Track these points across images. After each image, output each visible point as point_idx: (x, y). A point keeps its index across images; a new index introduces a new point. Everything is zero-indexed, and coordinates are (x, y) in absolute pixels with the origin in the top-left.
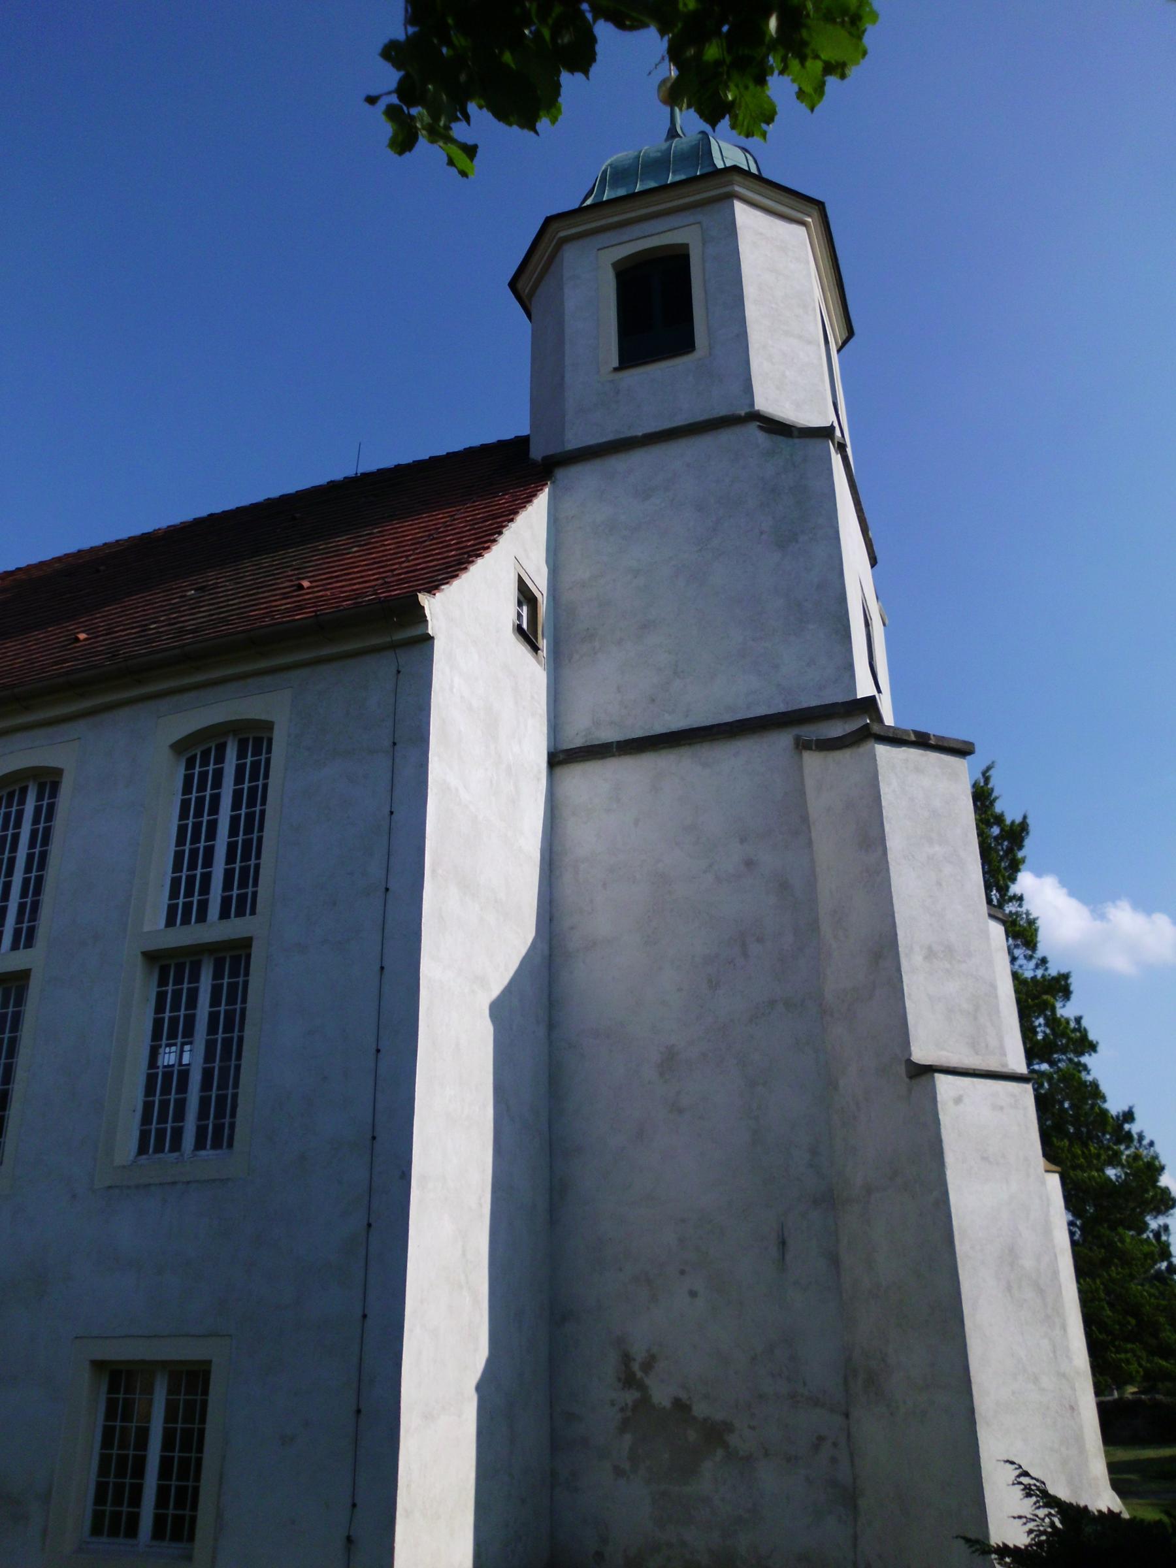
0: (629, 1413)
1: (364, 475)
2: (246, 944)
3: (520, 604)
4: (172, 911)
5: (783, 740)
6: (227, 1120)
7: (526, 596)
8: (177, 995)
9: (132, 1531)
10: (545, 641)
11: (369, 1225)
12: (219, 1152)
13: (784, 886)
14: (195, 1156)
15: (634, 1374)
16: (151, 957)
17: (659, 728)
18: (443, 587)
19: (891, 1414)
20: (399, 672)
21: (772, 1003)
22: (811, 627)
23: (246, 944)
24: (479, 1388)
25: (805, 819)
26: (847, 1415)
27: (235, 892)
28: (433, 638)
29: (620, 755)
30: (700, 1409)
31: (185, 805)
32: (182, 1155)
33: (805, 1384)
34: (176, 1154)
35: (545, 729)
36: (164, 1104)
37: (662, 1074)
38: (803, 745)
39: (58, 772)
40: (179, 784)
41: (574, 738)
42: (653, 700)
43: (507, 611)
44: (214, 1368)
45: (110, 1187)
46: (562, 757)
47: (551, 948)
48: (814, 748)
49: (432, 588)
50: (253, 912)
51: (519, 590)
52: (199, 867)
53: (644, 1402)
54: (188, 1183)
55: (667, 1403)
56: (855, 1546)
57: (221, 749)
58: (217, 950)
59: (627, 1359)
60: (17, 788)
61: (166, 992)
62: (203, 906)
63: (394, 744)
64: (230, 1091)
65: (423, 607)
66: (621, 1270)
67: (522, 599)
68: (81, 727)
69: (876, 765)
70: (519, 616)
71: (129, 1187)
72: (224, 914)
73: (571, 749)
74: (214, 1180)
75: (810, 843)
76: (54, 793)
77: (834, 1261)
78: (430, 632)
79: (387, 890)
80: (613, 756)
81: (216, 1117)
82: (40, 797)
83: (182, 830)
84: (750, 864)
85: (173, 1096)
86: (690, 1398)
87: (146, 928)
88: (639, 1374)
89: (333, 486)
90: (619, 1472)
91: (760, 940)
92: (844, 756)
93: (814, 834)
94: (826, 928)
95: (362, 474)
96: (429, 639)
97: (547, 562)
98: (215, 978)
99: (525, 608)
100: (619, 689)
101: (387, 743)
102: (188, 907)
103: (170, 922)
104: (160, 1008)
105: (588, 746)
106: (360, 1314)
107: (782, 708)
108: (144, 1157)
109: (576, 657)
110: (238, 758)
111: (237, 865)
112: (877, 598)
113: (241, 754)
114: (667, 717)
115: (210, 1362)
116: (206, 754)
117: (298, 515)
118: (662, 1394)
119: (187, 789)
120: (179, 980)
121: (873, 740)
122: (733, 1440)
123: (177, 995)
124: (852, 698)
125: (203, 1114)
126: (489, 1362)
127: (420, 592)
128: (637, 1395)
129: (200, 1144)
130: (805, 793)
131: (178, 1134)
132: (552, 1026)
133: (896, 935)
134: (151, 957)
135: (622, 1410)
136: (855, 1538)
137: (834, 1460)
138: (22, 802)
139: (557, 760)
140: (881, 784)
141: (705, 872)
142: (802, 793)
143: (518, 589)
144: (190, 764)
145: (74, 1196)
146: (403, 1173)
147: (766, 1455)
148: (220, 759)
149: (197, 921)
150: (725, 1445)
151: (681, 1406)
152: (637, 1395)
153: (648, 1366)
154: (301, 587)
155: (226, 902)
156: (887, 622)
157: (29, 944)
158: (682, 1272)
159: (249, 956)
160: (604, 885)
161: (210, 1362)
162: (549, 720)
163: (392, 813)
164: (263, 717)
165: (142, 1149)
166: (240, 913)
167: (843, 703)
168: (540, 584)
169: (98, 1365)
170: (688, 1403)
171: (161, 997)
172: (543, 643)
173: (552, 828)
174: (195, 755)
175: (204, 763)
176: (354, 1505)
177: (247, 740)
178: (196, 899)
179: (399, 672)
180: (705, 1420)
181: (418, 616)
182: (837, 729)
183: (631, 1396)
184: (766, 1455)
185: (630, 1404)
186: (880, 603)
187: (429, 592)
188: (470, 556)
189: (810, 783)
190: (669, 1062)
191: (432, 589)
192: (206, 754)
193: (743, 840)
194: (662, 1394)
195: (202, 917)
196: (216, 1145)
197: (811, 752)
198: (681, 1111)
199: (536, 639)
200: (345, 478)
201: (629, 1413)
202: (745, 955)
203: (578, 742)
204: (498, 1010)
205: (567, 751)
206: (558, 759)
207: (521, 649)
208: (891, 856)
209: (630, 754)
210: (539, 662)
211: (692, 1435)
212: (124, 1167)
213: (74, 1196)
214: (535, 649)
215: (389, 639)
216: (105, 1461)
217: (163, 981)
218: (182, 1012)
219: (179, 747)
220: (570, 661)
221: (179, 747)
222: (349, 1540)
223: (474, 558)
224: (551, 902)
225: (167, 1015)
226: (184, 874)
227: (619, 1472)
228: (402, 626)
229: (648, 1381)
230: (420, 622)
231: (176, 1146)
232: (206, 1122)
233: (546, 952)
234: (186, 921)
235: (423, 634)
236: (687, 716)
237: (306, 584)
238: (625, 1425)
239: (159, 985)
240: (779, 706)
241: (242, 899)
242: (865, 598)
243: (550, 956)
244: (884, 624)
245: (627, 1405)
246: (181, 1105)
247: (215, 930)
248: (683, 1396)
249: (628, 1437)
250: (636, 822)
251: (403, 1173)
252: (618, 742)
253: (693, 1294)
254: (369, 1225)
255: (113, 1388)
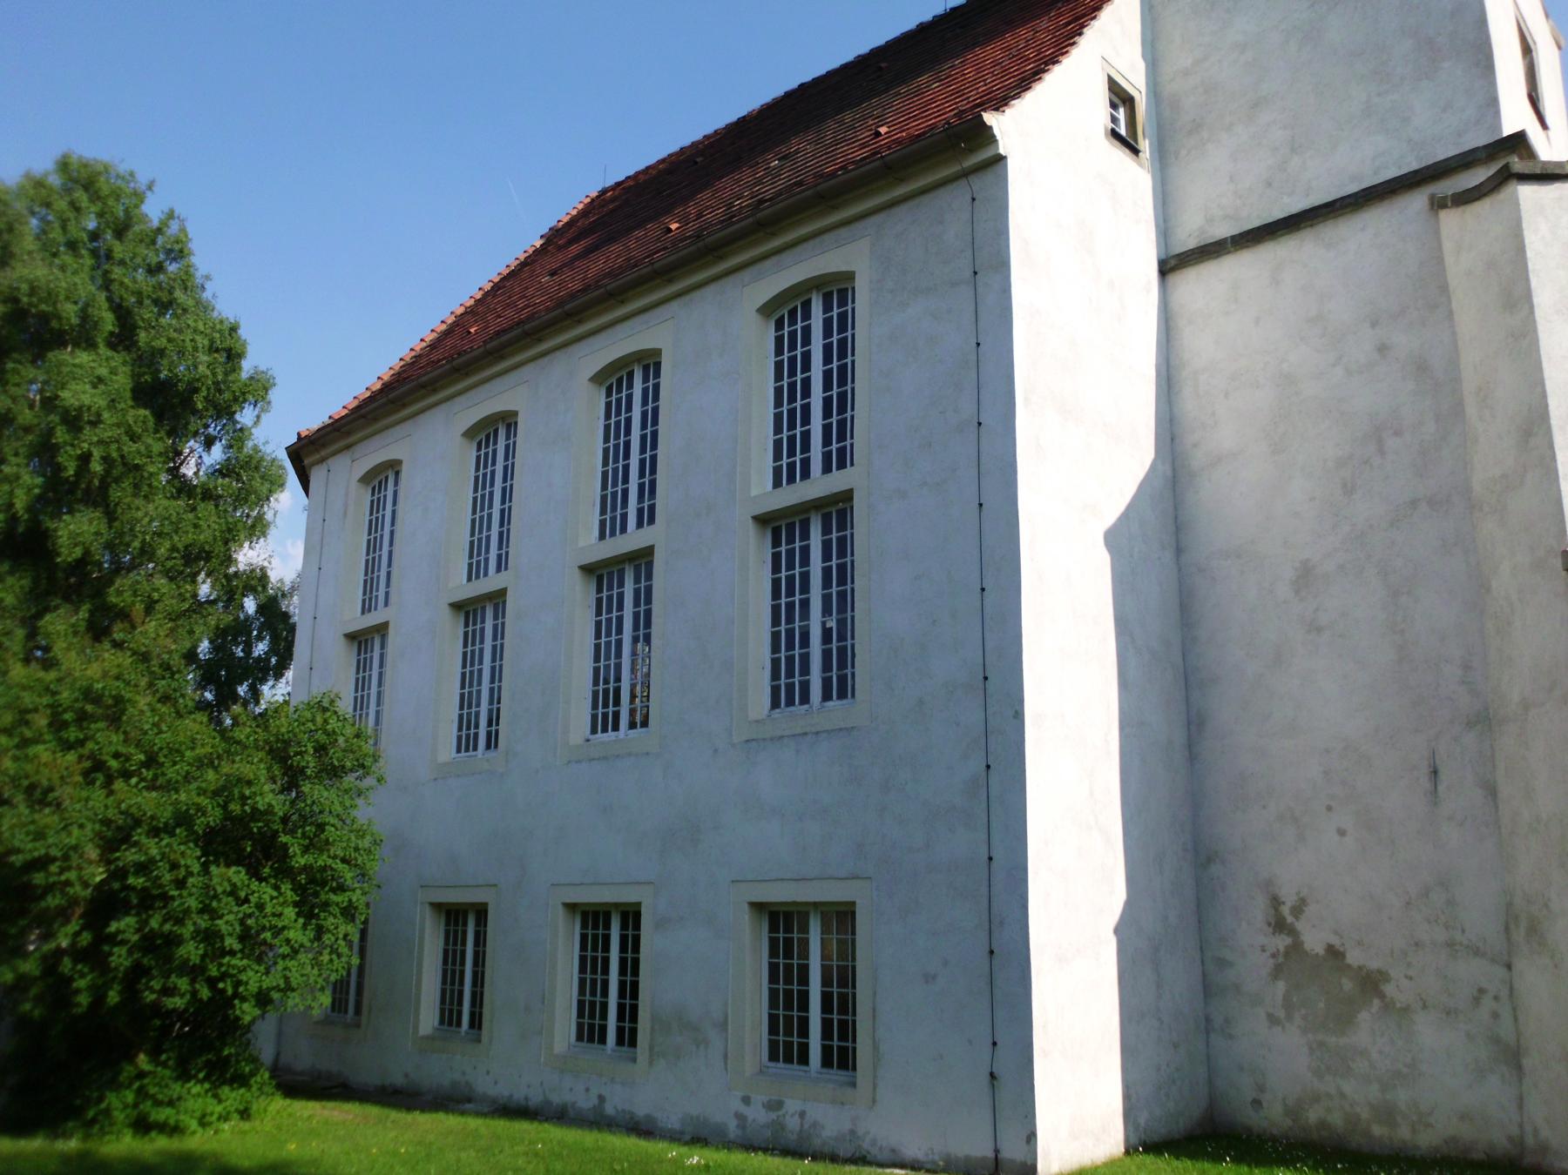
0: (1281, 960)
1: (954, 10)
2: (847, 496)
3: (1114, 106)
4: (777, 472)
5: (1417, 201)
6: (849, 671)
7: (1120, 97)
8: (791, 553)
9: (804, 1059)
10: (1147, 142)
11: (988, 767)
12: (844, 701)
13: (1421, 367)
14: (823, 707)
15: (1284, 919)
16: (762, 520)
17: (1279, 214)
18: (1013, 102)
19: (1556, 966)
20: (974, 199)
21: (1414, 503)
22: (1446, 65)
23: (847, 496)
24: (1116, 931)
25: (1444, 289)
26: (1509, 967)
27: (834, 446)
28: (1005, 157)
29: (1236, 250)
30: (1354, 957)
31: (779, 366)
32: (811, 707)
33: (1463, 931)
34: (806, 706)
35: (1153, 236)
36: (790, 660)
37: (1297, 592)
38: (1438, 204)
39: (657, 353)
40: (771, 346)
41: (1186, 240)
42: (1269, 185)
43: (1099, 112)
44: (643, 910)
45: (747, 741)
46: (1173, 262)
47: (1174, 470)
48: (1449, 204)
49: (1000, 102)
50: (852, 464)
51: (1110, 89)
52: (798, 426)
53: (1296, 947)
54: (817, 733)
55: (1320, 949)
56: (1521, 1106)
57: (807, 305)
58: (818, 505)
59: (1276, 902)
60: (624, 373)
61: (780, 553)
62: (806, 464)
63: (975, 273)
64: (849, 642)
65: (991, 128)
66: (1264, 807)
67: (1116, 100)
68: (675, 306)
69: (1519, 211)
70: (1114, 120)
71: (764, 739)
72: (827, 469)
73: (1182, 254)
74: (841, 729)
75: (1450, 314)
76: (657, 374)
77: (1492, 791)
78: (1002, 151)
79: (980, 424)
80: (1229, 252)
81: (838, 669)
82: (646, 379)
83: (778, 392)
84: (1382, 349)
85: (797, 652)
86: (1343, 944)
87: (754, 492)
88: (1290, 919)
89: (923, 29)
90: (1273, 1020)
91: (1397, 433)
92: (1483, 207)
93: (1454, 305)
94: (1471, 410)
95: (951, 9)
96: (1000, 159)
97: (1144, 56)
98: (824, 534)
99: (1122, 110)
100: (1232, 179)
101: (968, 273)
102: (791, 466)
103: (777, 483)
104: (776, 568)
105: (1202, 247)
106: (986, 857)
107: (1415, 166)
108: (777, 710)
109: (1183, 152)
110: (825, 312)
111: (834, 420)
112: (1547, 16)
113: (827, 308)
114: (1286, 200)
115: (639, 904)
116: (793, 313)
117: (883, 65)
118: (1314, 940)
119: (779, 350)
120: (791, 540)
121: (1515, 181)
122: (1389, 989)
123: (791, 553)
124: (1499, 138)
125: (826, 666)
126: (1129, 905)
127: (985, 110)
128: (1288, 941)
129: (827, 696)
130: (1443, 259)
131: (805, 687)
132: (1179, 551)
133: (1547, 406)
134: (762, 520)
135: (1273, 956)
136: (1521, 1098)
137: (1495, 1015)
138: (630, 386)
139: (1169, 266)
140: (1526, 233)
141: (1334, 365)
142: (1440, 260)
143: (1109, 89)
144: (779, 325)
145: (716, 751)
146: (1016, 712)
147: (1425, 1007)
148: (807, 315)
149: (801, 480)
150: (1382, 996)
151: (1334, 953)
152: (1288, 941)
153: (1298, 910)
154: (878, 134)
155: (827, 457)
156: (1563, 43)
157: (652, 520)
158: (1329, 808)
159: (852, 508)
160: (1226, 395)
161: (639, 904)
162: (1157, 226)
163: (978, 344)
164: (844, 269)
165: (775, 704)
166: (842, 465)
167: (1485, 147)
168: (1136, 81)
169: (758, 907)
170: (1342, 949)
171: (776, 558)
172: (1144, 145)
173: (1168, 341)
174: (783, 316)
175: (793, 322)
176: (994, 1044)
177: (831, 293)
178: (798, 458)
179: (974, 199)
180: (1360, 968)
181: (986, 136)
182: (1477, 176)
183: (1282, 942)
184: (1425, 1007)
185: (1282, 949)
186: (1550, 21)
187: (997, 109)
188: (1046, 65)
189: (1448, 246)
190: (1305, 576)
191: (1000, 103)
192: (793, 313)
193: (1374, 325)
194: (1314, 940)
195: (806, 474)
196: (842, 695)
197: (1448, 210)
198: (1319, 630)
199: (1136, 141)
200: (934, 17)
201: (1281, 960)
202: (1382, 452)
203: (1191, 244)
204: (1113, 538)
205: (1178, 255)
206: (1168, 267)
207: (1120, 155)
208: (1539, 314)
209: (1247, 247)
210: (1141, 165)
211: (1347, 984)
212: (757, 721)
213: (716, 751)
214: (1135, 151)
215: (959, 168)
216: (773, 995)
217: (776, 543)
218: (797, 570)
219: (766, 310)
220: (1176, 158)
221: (766, 310)
222: (992, 1075)
223: (1050, 66)
224: (1171, 420)
225: (783, 574)
226: (785, 435)
227: (1273, 1020)
228: (972, 150)
229: (1299, 926)
230: (989, 144)
231: (805, 699)
232: (830, 674)
233: (1169, 473)
234: (791, 479)
235: (994, 156)
236: (1308, 195)
237: (883, 130)
238: (1277, 972)
239: (774, 547)
240: (1412, 164)
241: (842, 452)
242: (1521, 14)
243: (1174, 477)
244: (1559, 48)
245: (1278, 950)
246: (805, 659)
247: (819, 485)
248: (1336, 941)
249: (1281, 986)
250: (1257, 321)
251: (1016, 712)
252: (1233, 237)
253: (1342, 833)
254: (988, 767)
255: (773, 928)
